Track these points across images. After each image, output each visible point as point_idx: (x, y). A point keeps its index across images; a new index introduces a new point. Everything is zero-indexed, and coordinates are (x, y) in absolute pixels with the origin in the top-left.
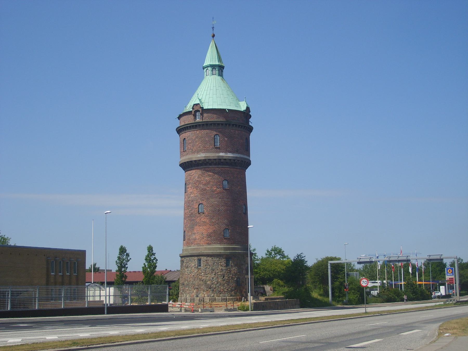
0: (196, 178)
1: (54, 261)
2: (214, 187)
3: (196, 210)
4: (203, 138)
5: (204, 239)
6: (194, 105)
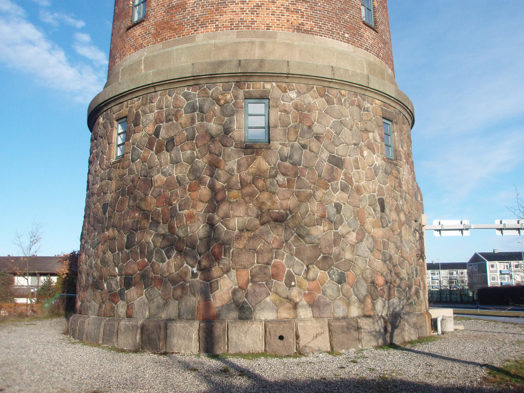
1: (180, 210)
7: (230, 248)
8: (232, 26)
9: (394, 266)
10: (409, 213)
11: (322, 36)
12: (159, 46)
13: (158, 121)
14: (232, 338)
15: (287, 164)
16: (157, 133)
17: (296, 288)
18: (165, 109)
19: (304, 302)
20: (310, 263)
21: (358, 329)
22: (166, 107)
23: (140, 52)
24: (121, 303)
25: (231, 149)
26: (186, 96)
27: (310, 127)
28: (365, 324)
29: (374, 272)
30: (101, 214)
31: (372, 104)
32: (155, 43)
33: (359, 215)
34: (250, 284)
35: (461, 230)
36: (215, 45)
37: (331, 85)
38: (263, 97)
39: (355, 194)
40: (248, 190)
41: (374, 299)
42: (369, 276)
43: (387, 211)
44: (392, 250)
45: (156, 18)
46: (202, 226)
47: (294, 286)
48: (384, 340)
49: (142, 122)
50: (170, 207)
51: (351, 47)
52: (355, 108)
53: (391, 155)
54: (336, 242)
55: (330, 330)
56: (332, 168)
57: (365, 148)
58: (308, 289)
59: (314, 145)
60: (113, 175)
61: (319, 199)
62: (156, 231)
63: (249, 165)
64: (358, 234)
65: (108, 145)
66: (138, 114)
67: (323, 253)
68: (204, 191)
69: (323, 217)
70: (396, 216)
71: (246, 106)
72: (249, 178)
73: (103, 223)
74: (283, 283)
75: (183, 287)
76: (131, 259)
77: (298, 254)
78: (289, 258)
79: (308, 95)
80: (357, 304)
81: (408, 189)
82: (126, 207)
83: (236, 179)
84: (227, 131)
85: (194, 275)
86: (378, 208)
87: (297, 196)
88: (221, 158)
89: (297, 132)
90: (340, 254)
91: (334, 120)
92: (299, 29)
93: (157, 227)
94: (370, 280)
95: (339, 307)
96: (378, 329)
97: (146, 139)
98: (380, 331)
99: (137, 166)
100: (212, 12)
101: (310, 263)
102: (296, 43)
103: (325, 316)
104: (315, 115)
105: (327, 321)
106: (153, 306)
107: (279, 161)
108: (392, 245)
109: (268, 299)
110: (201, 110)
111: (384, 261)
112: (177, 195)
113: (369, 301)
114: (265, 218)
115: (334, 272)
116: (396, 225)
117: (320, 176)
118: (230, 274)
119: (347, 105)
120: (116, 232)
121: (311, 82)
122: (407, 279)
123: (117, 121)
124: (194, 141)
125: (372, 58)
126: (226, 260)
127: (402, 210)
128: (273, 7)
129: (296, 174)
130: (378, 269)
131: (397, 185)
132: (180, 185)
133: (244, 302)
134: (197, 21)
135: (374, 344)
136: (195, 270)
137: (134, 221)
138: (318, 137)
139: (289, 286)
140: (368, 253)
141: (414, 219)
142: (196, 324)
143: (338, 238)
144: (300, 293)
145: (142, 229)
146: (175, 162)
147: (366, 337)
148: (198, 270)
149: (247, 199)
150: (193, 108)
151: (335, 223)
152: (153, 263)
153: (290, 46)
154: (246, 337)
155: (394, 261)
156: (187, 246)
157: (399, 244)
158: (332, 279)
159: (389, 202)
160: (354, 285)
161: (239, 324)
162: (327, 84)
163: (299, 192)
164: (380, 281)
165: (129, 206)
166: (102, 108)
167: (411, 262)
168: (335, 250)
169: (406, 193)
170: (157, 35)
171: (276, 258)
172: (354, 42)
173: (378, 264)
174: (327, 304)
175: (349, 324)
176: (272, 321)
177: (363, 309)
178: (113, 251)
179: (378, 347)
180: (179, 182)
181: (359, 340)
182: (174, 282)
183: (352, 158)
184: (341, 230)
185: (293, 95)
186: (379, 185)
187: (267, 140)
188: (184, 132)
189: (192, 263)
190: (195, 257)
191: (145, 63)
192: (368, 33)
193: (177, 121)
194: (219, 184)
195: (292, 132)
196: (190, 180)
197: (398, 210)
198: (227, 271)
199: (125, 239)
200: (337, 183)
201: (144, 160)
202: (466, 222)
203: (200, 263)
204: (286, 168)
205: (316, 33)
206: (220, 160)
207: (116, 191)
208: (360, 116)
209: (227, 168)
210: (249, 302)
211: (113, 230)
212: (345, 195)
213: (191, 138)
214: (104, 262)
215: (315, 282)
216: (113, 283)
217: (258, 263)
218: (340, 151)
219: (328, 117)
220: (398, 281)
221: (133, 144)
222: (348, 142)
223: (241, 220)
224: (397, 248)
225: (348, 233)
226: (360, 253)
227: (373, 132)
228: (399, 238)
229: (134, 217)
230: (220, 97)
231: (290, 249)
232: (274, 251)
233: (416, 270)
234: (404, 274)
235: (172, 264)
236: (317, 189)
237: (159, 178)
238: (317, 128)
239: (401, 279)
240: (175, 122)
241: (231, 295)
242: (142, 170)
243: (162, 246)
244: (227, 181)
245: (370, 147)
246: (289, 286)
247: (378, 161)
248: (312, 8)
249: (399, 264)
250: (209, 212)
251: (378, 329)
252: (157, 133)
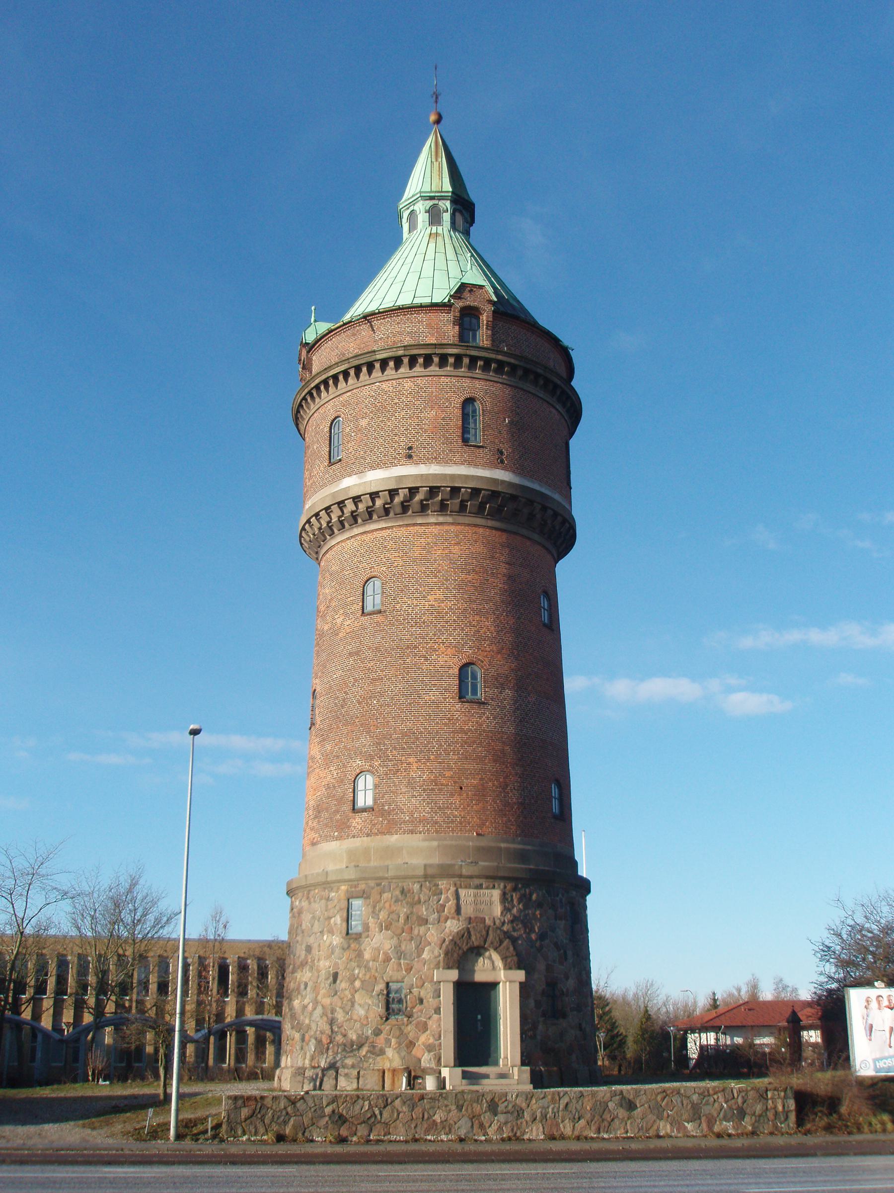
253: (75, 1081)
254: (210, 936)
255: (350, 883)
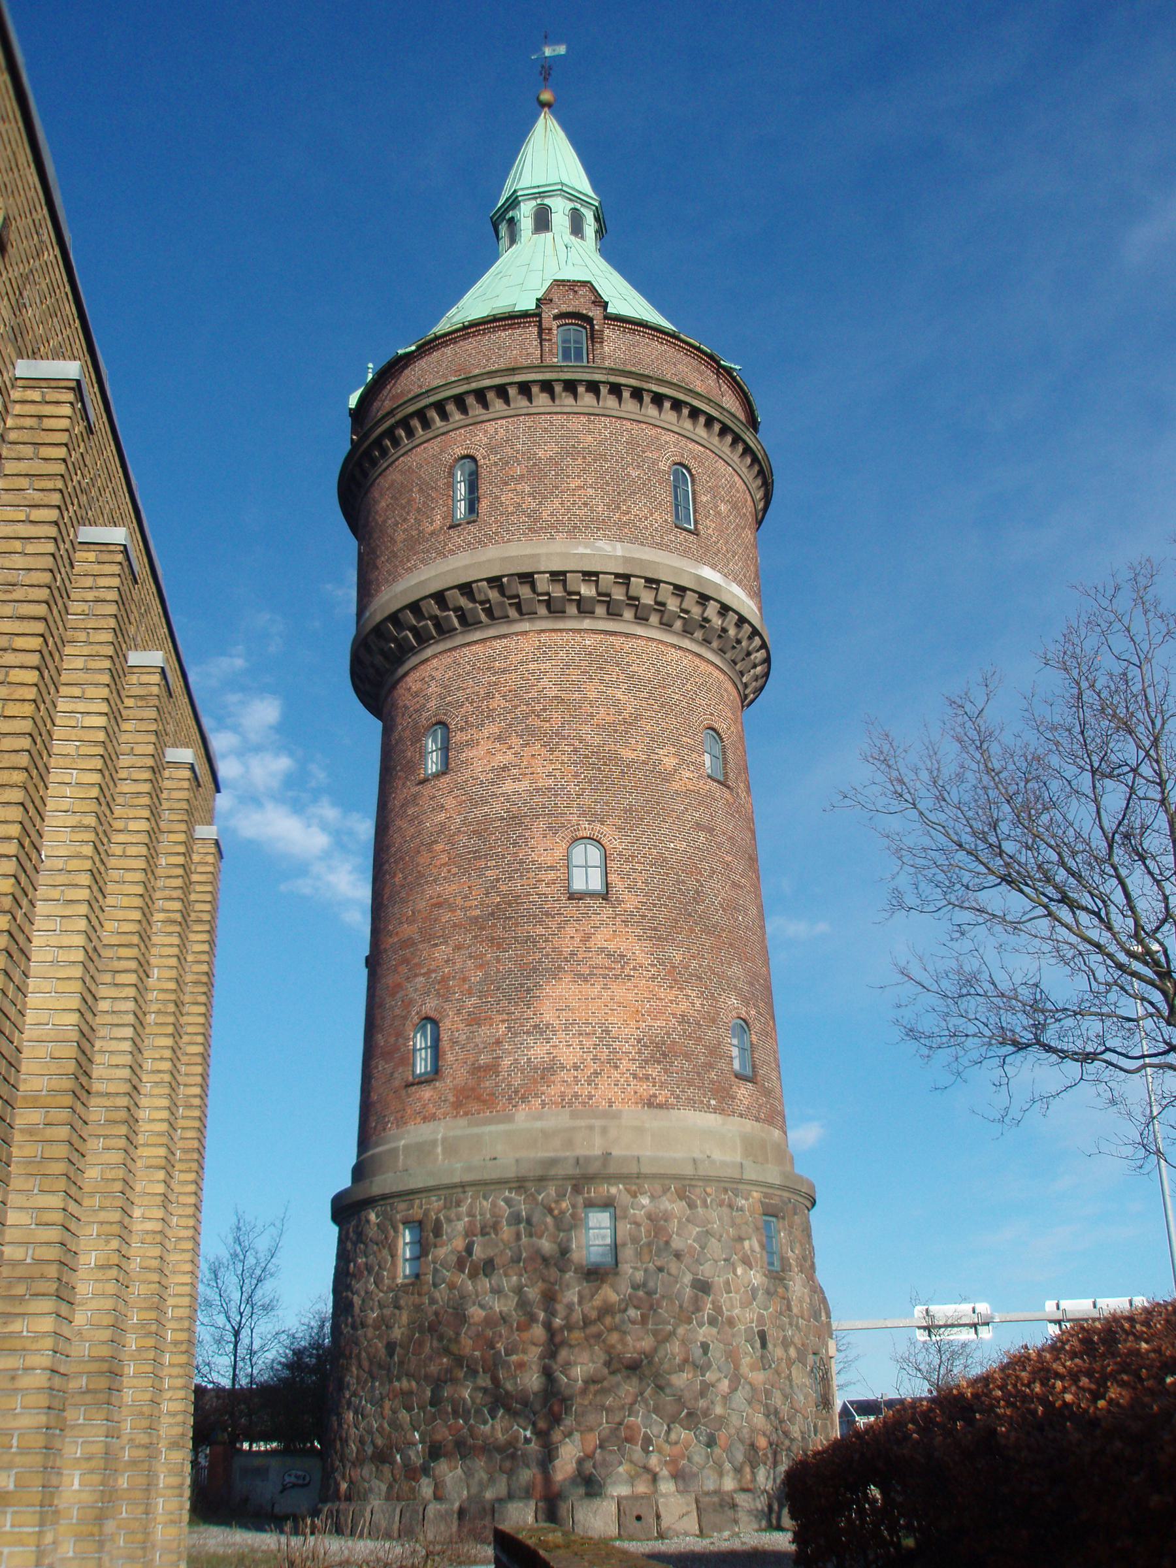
0: (545, 682)
1: (506, 1355)
2: (661, 752)
3: (552, 875)
4: (606, 461)
5: (616, 1067)
6: (558, 283)
7: (572, 1405)
8: (564, 1102)
9: (781, 1422)
10: (803, 1345)
11: (679, 1109)
12: (462, 1122)
13: (469, 1233)
14: (579, 1521)
15: (641, 1293)
16: (469, 1249)
17: (655, 1454)
18: (478, 1217)
19: (665, 1472)
20: (672, 1420)
21: (734, 1506)
22: (481, 1215)
23: (431, 1125)
24: (424, 1481)
25: (569, 1275)
26: (508, 1201)
27: (667, 1243)
28: (742, 1499)
29: (753, 1430)
30: (383, 1357)
31: (747, 1199)
32: (456, 1117)
33: (732, 1356)
34: (598, 1451)
35: (974, 1326)
36: (543, 1131)
37: (693, 1183)
38: (607, 1204)
39: (727, 1328)
40: (593, 1329)
41: (753, 1467)
42: (747, 1436)
43: (770, 1346)
44: (777, 1400)
45: (455, 1078)
46: (535, 1376)
47: (652, 1451)
48: (769, 1521)
49: (447, 1233)
50: (492, 1352)
51: (718, 1116)
52: (725, 1209)
53: (777, 1266)
54: (702, 1394)
55: (698, 1508)
56: (697, 1295)
57: (740, 1263)
58: (669, 1456)
59: (673, 1267)
60: (402, 1302)
61: (680, 1338)
62: (474, 1382)
63: (593, 1296)
64: (730, 1380)
65: (389, 1257)
66: (438, 1220)
67: (688, 1409)
68: (538, 1331)
69: (686, 1361)
70: (783, 1352)
71: (587, 1217)
72: (594, 1315)
73: (389, 1370)
74: (639, 1448)
75: (513, 1456)
76: (439, 1421)
77: (656, 1410)
78: (646, 1417)
79: (664, 1198)
80: (731, 1474)
81: (802, 1311)
82: (427, 1349)
83: (577, 1316)
84: (564, 1251)
85: (527, 1441)
86: (758, 1345)
87: (653, 1335)
88: (557, 1287)
89: (651, 1251)
90: (708, 1409)
91: (698, 1229)
92: (650, 1103)
93: (475, 1377)
94: (748, 1441)
95: (708, 1478)
96: (760, 1507)
97: (455, 1259)
98: (762, 1511)
99: (442, 1294)
100: (535, 1082)
101: (672, 1420)
102: (647, 1125)
103: (692, 1489)
104: (674, 1225)
105: (694, 1496)
106: (474, 1483)
107: (630, 1290)
108: (777, 1394)
109: (621, 1469)
110: (529, 1222)
111: (767, 1416)
112: (501, 1336)
113: (747, 1469)
114: (615, 1365)
115: (701, 1432)
116: (784, 1365)
117: (681, 1307)
118: (572, 1437)
119: (715, 1207)
120: (414, 1384)
121: (667, 1182)
122: (800, 1438)
123: (404, 1224)
124: (522, 1264)
125: (749, 1125)
126: (569, 1422)
127: (792, 1342)
128: (616, 1074)
129: (651, 1307)
130: (759, 1427)
131: (784, 1308)
132: (505, 1322)
133: (591, 1474)
134: (516, 1092)
135: (756, 1526)
136: (528, 1434)
137: (440, 1370)
138: (678, 1256)
139: (647, 1452)
140: (744, 1406)
141: (810, 1352)
142: (532, 1504)
143: (705, 1389)
144: (660, 1461)
145: (454, 1381)
146: (497, 1291)
147: (742, 1516)
148: (532, 1433)
149: (592, 1341)
150: (516, 1219)
151: (701, 1369)
152: (471, 1425)
153: (640, 1130)
154: (595, 1517)
155: (781, 1415)
156: (516, 1403)
157: (788, 1390)
158: (699, 1441)
159: (772, 1333)
160: (728, 1450)
161: (586, 1502)
162: (687, 1182)
163: (656, 1330)
164: (762, 1442)
165: (431, 1347)
166: (376, 1201)
167: (806, 1415)
168: (702, 1403)
169: (798, 1317)
170: (457, 1105)
171: (629, 1416)
172: (723, 1110)
173: (759, 1420)
174: (695, 1475)
175: (722, 1500)
176: (626, 1498)
177: (740, 1481)
178: (409, 1409)
179: (761, 1530)
180: (503, 1318)
181: (736, 1522)
182: (500, 1449)
183: (721, 1279)
184: (710, 1376)
185: (645, 1201)
186: (759, 1312)
187: (614, 1262)
188: (507, 1251)
189: (523, 1425)
190: (527, 1417)
191: (442, 1144)
192: (743, 1091)
193: (497, 1235)
194: (558, 1322)
195: (645, 1250)
196: (518, 1315)
197: (786, 1344)
198: (569, 1435)
199: (429, 1394)
200: (703, 1316)
201: (452, 1286)
202: (983, 1308)
203: (534, 1424)
204: (640, 1299)
205: (673, 1107)
206: (556, 1291)
207: (408, 1325)
208: (732, 1219)
209: (565, 1301)
210: (599, 1473)
211: (409, 1381)
212: (714, 1331)
213: (517, 1260)
214: (395, 1424)
215: (679, 1446)
216: (412, 1454)
217: (607, 1422)
218: (706, 1270)
219: (690, 1226)
220: (787, 1442)
221: (434, 1262)
222: (716, 1258)
223: (585, 1368)
224: (786, 1397)
225: (719, 1380)
226: (734, 1406)
227: (749, 1239)
228: (787, 1383)
229: (442, 1364)
230: (553, 1205)
231: (647, 1405)
232: (627, 1407)
233: (815, 1427)
234: (795, 1431)
235: (498, 1427)
236: (678, 1325)
237: (476, 1313)
238: (677, 1243)
239: (792, 1440)
240: (494, 1236)
241: (574, 1465)
242: (449, 1299)
243: (483, 1403)
244: (567, 1318)
245: (747, 1262)
246: (647, 1452)
247: (756, 1278)
248: (666, 1071)
249: (788, 1419)
250: (544, 1358)
251: (760, 1507)
252: (469, 1249)
253: (338, 1531)
254: (604, 1237)
255: (765, 1190)
